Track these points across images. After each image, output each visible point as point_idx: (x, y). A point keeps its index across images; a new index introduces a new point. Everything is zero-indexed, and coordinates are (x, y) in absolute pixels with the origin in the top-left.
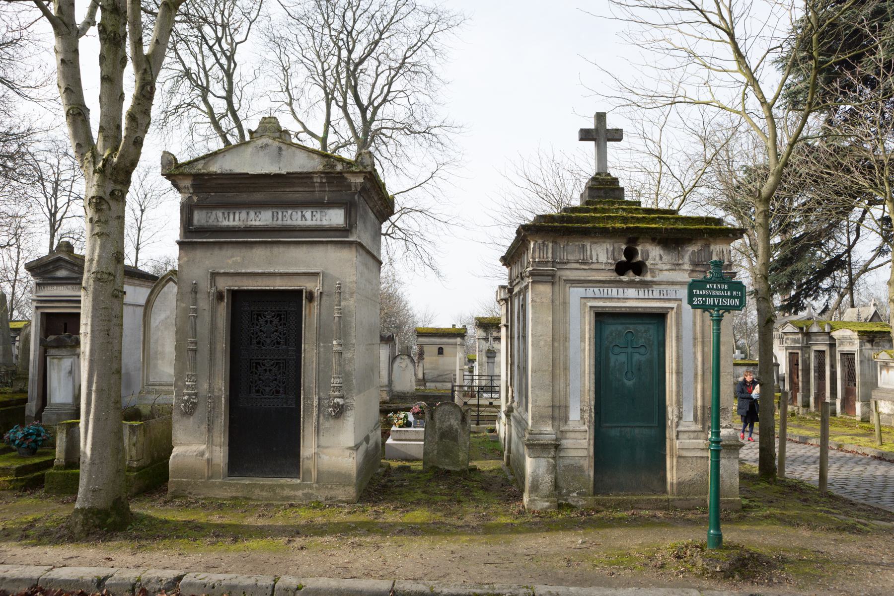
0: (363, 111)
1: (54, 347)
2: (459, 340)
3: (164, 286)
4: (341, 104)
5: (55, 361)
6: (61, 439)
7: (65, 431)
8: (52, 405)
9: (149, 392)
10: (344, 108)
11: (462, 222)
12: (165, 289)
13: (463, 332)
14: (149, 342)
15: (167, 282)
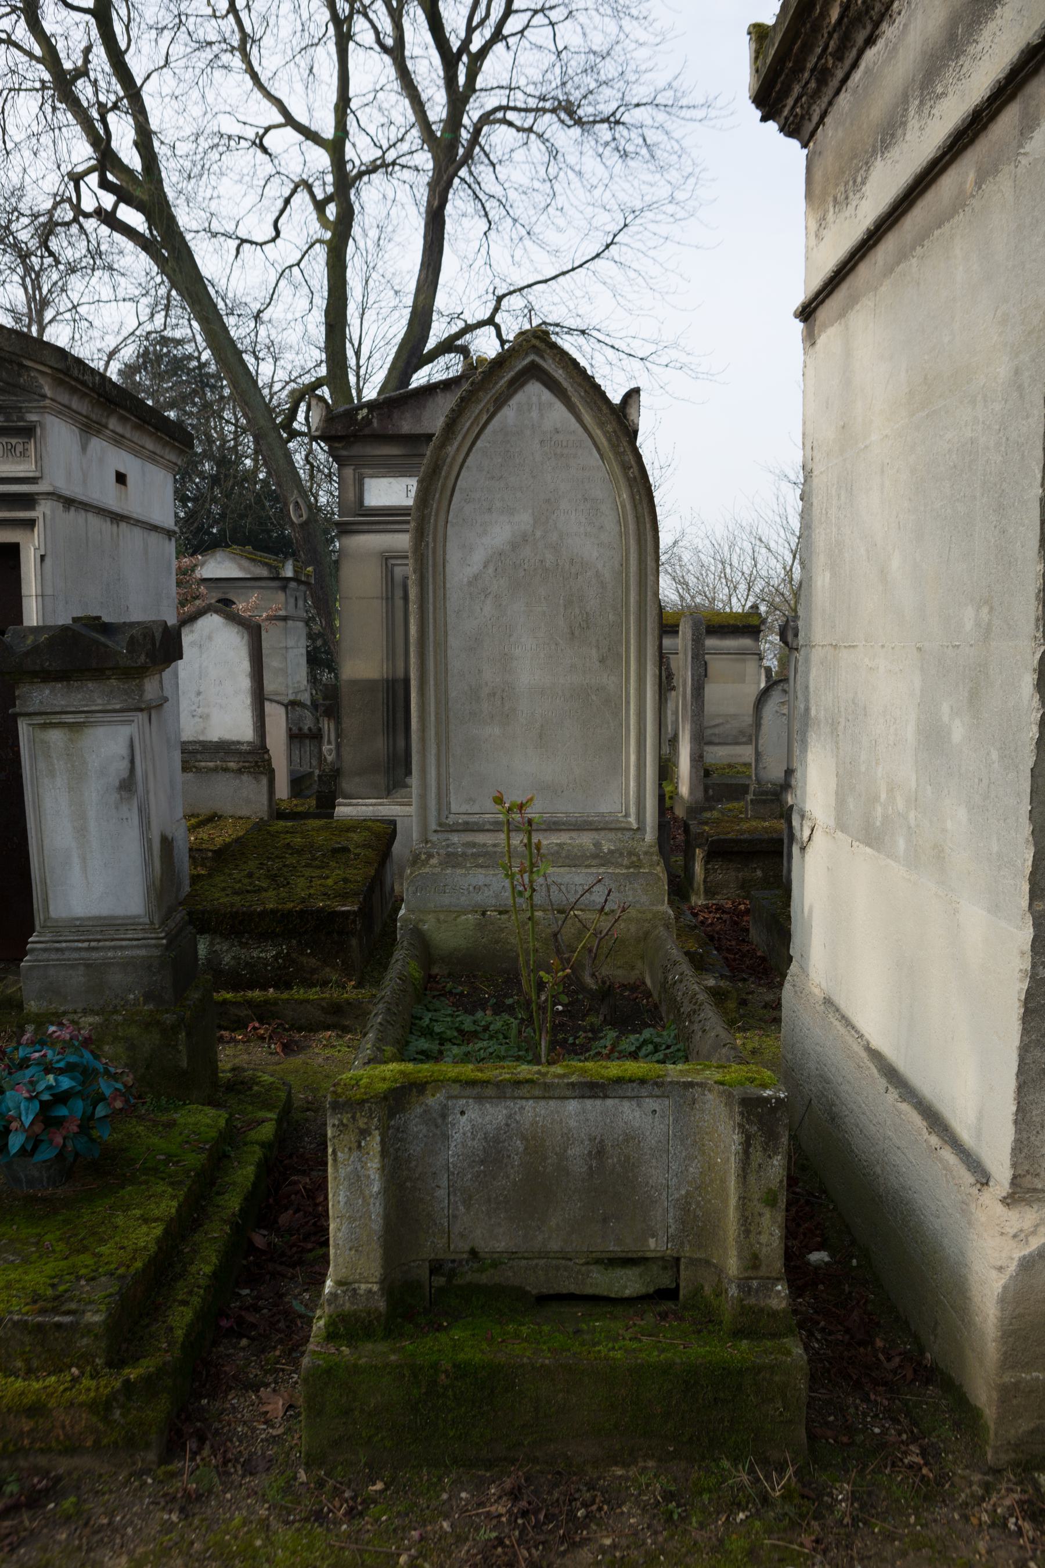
0: (450, 60)
1: (47, 677)
2: (746, 642)
3: (500, 402)
4: (389, 42)
5: (56, 737)
6: (357, 1181)
7: (374, 1142)
8: (59, 928)
9: (452, 860)
10: (397, 52)
11: (684, 359)
12: (509, 414)
13: (755, 621)
14: (442, 646)
15: (517, 384)
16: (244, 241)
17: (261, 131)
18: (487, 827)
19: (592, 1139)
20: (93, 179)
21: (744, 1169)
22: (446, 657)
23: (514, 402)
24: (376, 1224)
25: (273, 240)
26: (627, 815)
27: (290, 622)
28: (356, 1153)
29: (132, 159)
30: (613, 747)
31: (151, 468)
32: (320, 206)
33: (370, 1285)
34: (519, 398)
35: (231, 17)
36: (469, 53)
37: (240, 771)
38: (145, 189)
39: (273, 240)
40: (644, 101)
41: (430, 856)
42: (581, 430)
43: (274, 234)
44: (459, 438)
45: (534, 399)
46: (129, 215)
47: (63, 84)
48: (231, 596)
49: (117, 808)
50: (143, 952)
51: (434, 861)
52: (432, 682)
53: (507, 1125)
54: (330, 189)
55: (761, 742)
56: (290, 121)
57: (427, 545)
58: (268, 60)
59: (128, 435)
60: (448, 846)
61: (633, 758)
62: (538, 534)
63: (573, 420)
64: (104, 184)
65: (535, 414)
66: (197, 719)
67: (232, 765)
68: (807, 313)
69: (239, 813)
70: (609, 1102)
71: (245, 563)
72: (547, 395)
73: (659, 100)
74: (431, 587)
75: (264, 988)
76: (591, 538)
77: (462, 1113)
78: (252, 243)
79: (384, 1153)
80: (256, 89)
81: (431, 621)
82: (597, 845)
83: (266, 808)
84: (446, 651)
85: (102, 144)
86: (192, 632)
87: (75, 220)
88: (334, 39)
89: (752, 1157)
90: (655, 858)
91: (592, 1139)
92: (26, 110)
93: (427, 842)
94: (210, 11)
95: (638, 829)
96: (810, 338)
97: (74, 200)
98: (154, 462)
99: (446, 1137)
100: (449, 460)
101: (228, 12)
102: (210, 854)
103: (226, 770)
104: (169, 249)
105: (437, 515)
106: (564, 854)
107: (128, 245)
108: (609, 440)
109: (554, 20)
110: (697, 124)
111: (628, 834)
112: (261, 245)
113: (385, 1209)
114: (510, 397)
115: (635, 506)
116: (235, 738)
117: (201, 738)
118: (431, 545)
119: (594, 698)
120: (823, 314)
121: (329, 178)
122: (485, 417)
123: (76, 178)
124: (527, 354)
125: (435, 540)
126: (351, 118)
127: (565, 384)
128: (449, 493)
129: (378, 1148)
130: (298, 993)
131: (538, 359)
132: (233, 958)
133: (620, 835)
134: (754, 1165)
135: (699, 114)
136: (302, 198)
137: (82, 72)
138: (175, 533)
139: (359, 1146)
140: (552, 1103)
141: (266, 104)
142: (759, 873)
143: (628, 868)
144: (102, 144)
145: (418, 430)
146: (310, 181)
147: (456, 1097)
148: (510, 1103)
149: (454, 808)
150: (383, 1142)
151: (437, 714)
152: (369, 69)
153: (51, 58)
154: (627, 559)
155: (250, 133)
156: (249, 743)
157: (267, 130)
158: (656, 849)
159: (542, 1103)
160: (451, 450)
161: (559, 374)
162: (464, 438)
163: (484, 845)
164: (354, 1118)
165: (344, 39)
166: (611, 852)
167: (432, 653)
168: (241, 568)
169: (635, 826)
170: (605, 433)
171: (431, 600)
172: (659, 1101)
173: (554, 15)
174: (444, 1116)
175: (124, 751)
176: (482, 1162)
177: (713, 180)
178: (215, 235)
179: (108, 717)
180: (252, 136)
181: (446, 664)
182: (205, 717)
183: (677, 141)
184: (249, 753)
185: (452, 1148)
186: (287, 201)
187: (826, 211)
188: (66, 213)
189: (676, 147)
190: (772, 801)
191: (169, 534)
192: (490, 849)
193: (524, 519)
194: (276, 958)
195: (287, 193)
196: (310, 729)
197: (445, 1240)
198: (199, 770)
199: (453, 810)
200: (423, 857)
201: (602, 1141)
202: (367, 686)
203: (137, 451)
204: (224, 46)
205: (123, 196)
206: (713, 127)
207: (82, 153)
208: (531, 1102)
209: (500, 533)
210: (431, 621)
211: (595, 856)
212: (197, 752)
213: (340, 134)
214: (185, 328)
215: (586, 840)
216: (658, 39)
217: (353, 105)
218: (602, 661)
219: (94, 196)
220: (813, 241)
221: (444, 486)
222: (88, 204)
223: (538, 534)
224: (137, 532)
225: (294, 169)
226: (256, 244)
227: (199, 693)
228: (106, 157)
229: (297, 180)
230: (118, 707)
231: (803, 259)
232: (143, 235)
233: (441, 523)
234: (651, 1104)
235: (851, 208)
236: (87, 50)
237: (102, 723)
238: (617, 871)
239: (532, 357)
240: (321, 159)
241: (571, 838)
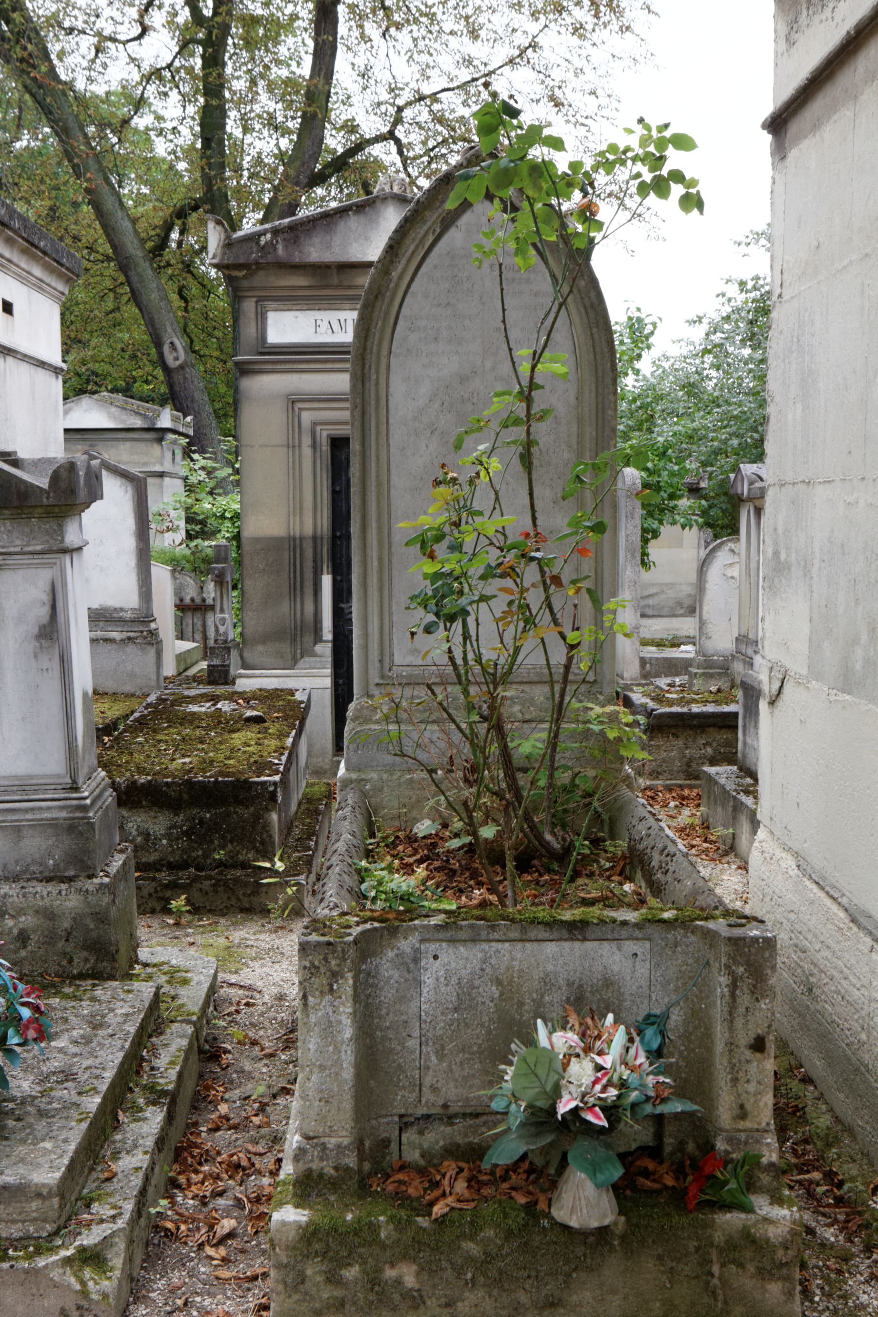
7: (347, 984)
19: (570, 984)
21: (730, 1013)
24: (348, 1073)
27: (167, 480)
28: (328, 997)
31: (37, 296)
33: (341, 1136)
44: (403, 262)
49: (36, 657)
50: (64, 814)
53: (482, 970)
59: (15, 260)
62: (488, 365)
68: (778, 124)
70: (589, 945)
77: (436, 957)
79: (356, 998)
81: (373, 459)
89: (739, 1000)
91: (570, 984)
96: (780, 151)
98: (41, 290)
99: (419, 983)
100: (392, 285)
113: (356, 1057)
116: (117, 605)
120: (793, 128)
122: (431, 239)
129: (349, 990)
134: (741, 1010)
138: (62, 370)
139: (331, 990)
140: (528, 945)
145: (328, 257)
147: (428, 940)
148: (485, 946)
149: (398, 660)
150: (355, 987)
159: (519, 945)
164: (325, 959)
168: (112, 417)
172: (640, 943)
174: (416, 960)
175: (45, 597)
176: (456, 1010)
179: (26, 560)
185: (425, 994)
187: (798, 13)
190: (719, 674)
191: (57, 371)
196: (192, 600)
197: (415, 1095)
201: (581, 986)
202: (273, 545)
203: (24, 278)
208: (507, 945)
220: (783, 45)
221: (387, 313)
224: (24, 367)
230: (39, 548)
231: (772, 65)
233: (385, 352)
234: (631, 947)
235: (828, 11)
237: (21, 566)
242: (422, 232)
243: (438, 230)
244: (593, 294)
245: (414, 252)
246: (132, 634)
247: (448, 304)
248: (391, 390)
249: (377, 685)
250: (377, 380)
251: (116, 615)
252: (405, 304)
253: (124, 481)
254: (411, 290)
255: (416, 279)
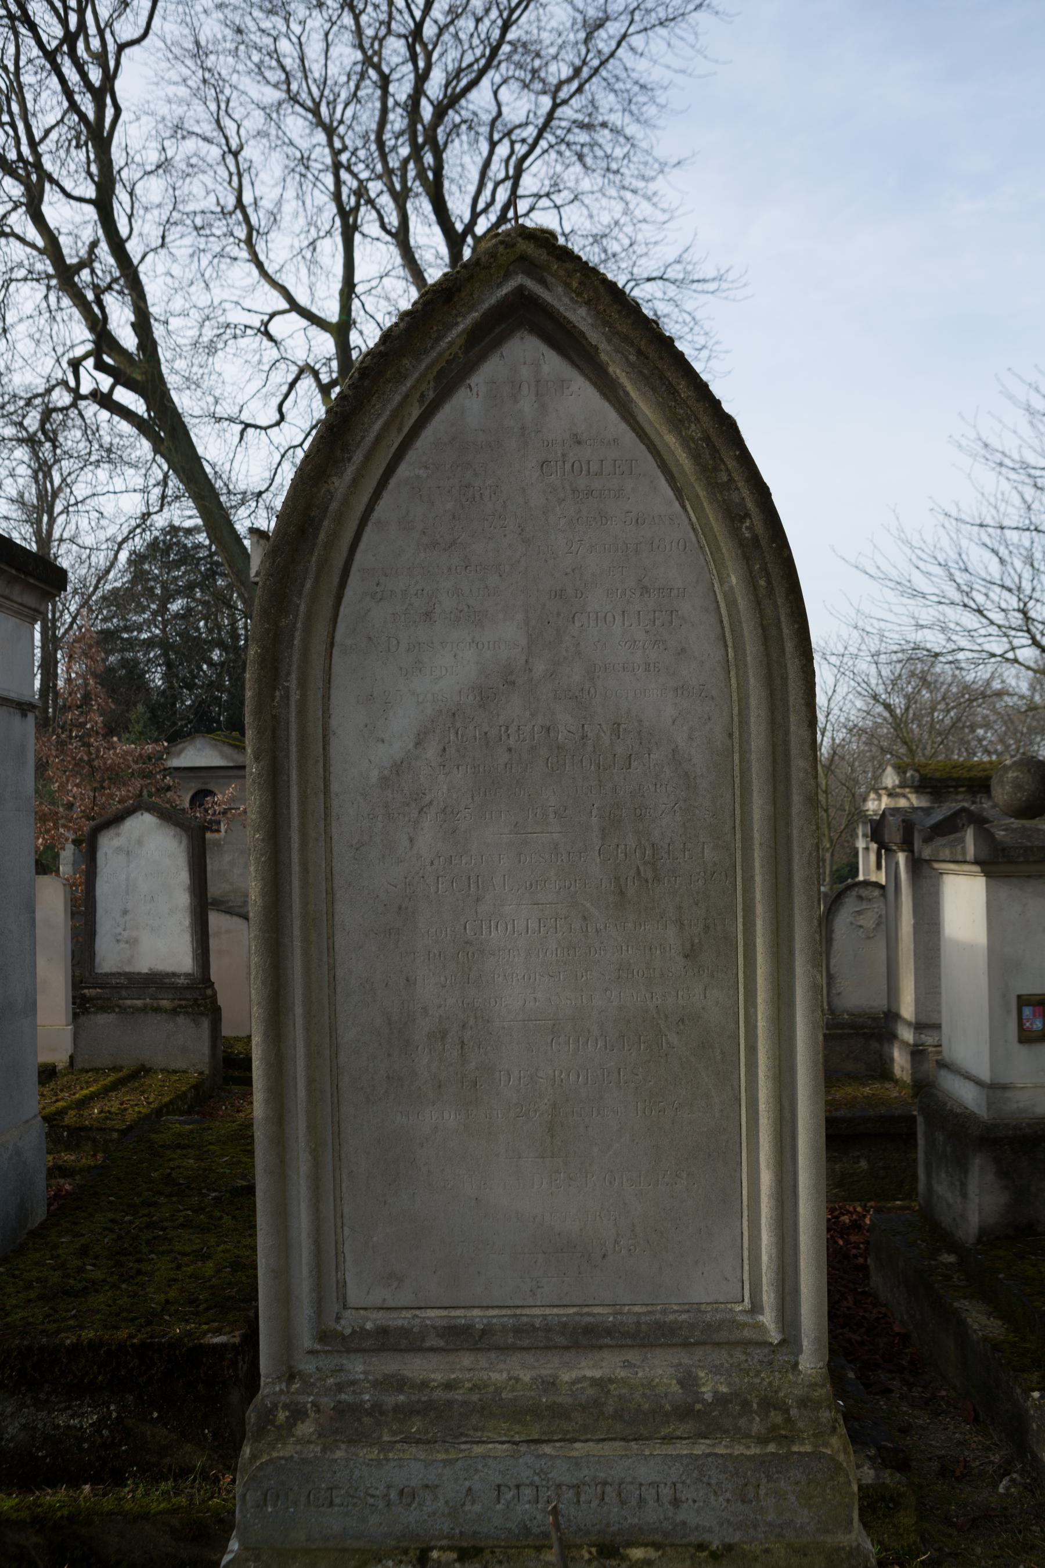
10: (401, 237)
12: (469, 405)
15: (486, 338)
16: (248, 425)
17: (266, 318)
18: (432, 1341)
20: (90, 363)
22: (331, 949)
23: (479, 379)
25: (277, 424)
26: (756, 1308)
29: (129, 340)
30: (722, 1150)
32: (324, 390)
34: (491, 369)
35: (238, 212)
36: (474, 236)
37: (174, 1012)
38: (142, 370)
39: (277, 424)
40: (654, 275)
41: (298, 1414)
42: (629, 437)
43: (277, 417)
44: (358, 457)
45: (525, 372)
46: (124, 396)
47: (65, 276)
48: (211, 786)
51: (306, 1428)
52: (299, 1010)
54: (335, 375)
55: (833, 962)
56: (295, 306)
57: (287, 697)
58: (277, 251)
60: (340, 1388)
61: (766, 1178)
62: (540, 668)
63: (612, 415)
64: (100, 366)
65: (527, 405)
66: (123, 945)
67: (165, 1003)
69: (173, 1065)
71: (227, 750)
72: (552, 363)
73: (670, 274)
74: (294, 791)
75: (75, 1483)
76: (657, 679)
78: (256, 427)
80: (263, 281)
82: (688, 1381)
83: (207, 1060)
84: (331, 936)
85: (99, 326)
86: (118, 835)
87: (74, 405)
88: (340, 230)
90: (826, 1415)
92: (27, 297)
93: (291, 1377)
94: (219, 209)
95: (783, 1342)
97: (72, 383)
100: (334, 505)
101: (236, 208)
102: (115, 1135)
103: (157, 1010)
104: (167, 431)
105: (308, 629)
106: (610, 1410)
107: (125, 427)
108: (696, 457)
109: (559, 202)
110: (709, 295)
111: (758, 1354)
112: (265, 429)
114: (469, 368)
115: (758, 604)
116: (169, 969)
117: (127, 969)
118: (295, 697)
119: (674, 1039)
121: (334, 364)
122: (416, 413)
123: (75, 365)
124: (507, 276)
125: (303, 684)
126: (356, 304)
127: (594, 336)
128: (335, 580)
130: (132, 1495)
131: (530, 284)
132: (24, 1427)
133: (739, 1356)
135: (712, 286)
136: (307, 383)
137: (88, 262)
141: (275, 294)
142: (864, 1164)
143: (763, 1441)
144: (99, 326)
146: (317, 367)
149: (354, 1295)
151: (311, 1081)
152: (375, 256)
153: (52, 248)
154: (743, 722)
155: (256, 321)
156: (186, 975)
157: (272, 316)
158: (824, 1391)
160: (340, 484)
161: (580, 317)
162: (368, 457)
163: (424, 1384)
165: (349, 232)
166: (721, 1400)
167: (297, 943)
168: (224, 756)
169: (775, 1337)
170: (686, 442)
171: (295, 822)
173: (558, 199)
177: (727, 352)
178: (219, 420)
180: (258, 324)
181: (332, 968)
182: (133, 942)
183: (690, 314)
184: (187, 988)
186: (292, 385)
188: (61, 398)
189: (688, 319)
192: (439, 1395)
193: (507, 635)
194: (97, 1426)
195: (291, 378)
198: (123, 1010)
199: (353, 1299)
200: (282, 1416)
204: (232, 239)
205: (120, 378)
206: (726, 298)
207: (79, 335)
209: (452, 668)
210: (296, 868)
211: (684, 1412)
212: (122, 987)
213: (344, 317)
214: (184, 514)
215: (659, 1370)
216: (666, 217)
217: (359, 289)
218: (690, 954)
219: (92, 379)
222: (85, 389)
223: (540, 668)
225: (300, 356)
226: (261, 428)
227: (125, 912)
228: (103, 338)
229: (301, 363)
232: (141, 417)
233: (318, 647)
236: (94, 244)
238: (738, 1450)
239: (519, 279)
240: (325, 344)
241: (627, 1365)
242: (397, 398)
243: (431, 395)
244: (757, 519)
245: (378, 439)
246: (183, 1003)
247: (453, 543)
248: (334, 723)
249: (311, 1352)
250: (303, 703)
251: (167, 981)
252: (362, 546)
253: (178, 829)
254: (375, 515)
255: (386, 495)
